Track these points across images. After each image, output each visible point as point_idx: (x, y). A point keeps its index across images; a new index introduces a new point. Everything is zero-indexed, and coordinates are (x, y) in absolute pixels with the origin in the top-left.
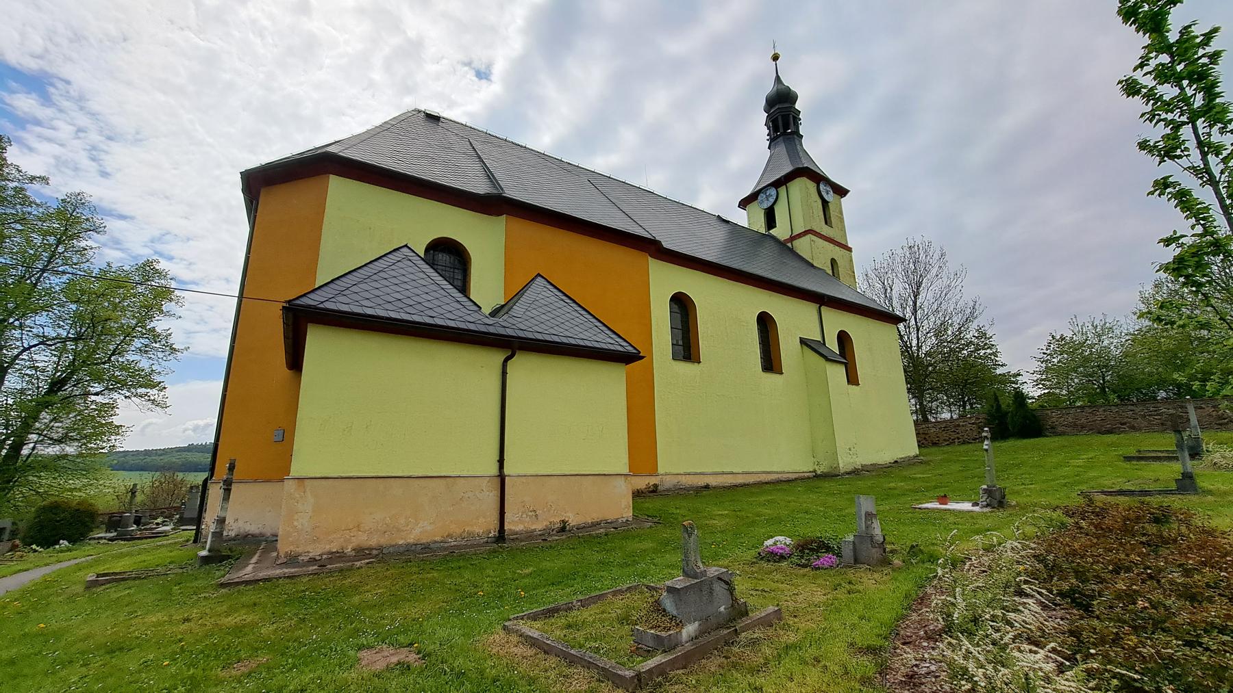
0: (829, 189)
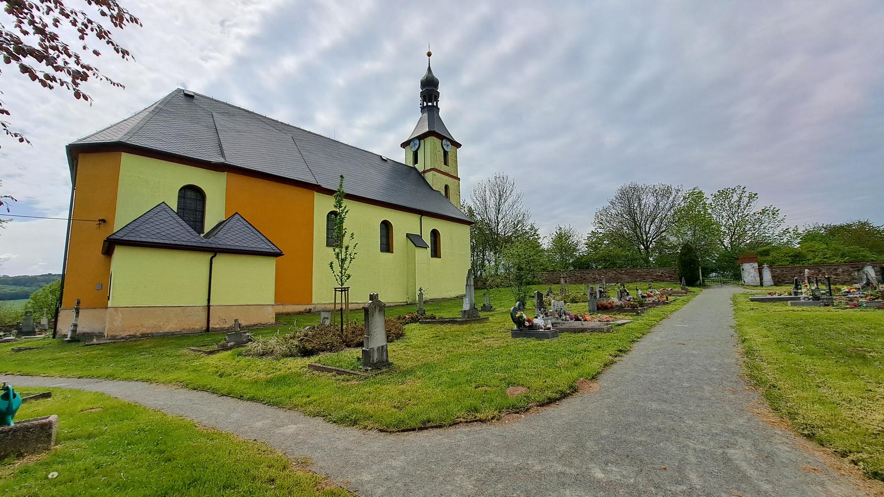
0: (449, 143)
